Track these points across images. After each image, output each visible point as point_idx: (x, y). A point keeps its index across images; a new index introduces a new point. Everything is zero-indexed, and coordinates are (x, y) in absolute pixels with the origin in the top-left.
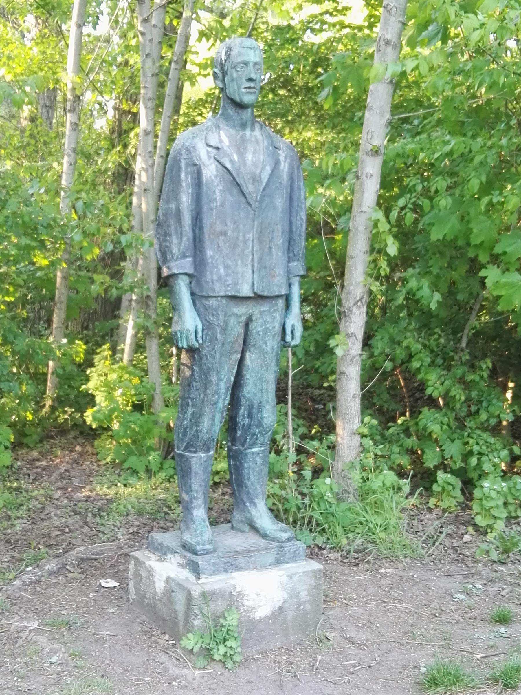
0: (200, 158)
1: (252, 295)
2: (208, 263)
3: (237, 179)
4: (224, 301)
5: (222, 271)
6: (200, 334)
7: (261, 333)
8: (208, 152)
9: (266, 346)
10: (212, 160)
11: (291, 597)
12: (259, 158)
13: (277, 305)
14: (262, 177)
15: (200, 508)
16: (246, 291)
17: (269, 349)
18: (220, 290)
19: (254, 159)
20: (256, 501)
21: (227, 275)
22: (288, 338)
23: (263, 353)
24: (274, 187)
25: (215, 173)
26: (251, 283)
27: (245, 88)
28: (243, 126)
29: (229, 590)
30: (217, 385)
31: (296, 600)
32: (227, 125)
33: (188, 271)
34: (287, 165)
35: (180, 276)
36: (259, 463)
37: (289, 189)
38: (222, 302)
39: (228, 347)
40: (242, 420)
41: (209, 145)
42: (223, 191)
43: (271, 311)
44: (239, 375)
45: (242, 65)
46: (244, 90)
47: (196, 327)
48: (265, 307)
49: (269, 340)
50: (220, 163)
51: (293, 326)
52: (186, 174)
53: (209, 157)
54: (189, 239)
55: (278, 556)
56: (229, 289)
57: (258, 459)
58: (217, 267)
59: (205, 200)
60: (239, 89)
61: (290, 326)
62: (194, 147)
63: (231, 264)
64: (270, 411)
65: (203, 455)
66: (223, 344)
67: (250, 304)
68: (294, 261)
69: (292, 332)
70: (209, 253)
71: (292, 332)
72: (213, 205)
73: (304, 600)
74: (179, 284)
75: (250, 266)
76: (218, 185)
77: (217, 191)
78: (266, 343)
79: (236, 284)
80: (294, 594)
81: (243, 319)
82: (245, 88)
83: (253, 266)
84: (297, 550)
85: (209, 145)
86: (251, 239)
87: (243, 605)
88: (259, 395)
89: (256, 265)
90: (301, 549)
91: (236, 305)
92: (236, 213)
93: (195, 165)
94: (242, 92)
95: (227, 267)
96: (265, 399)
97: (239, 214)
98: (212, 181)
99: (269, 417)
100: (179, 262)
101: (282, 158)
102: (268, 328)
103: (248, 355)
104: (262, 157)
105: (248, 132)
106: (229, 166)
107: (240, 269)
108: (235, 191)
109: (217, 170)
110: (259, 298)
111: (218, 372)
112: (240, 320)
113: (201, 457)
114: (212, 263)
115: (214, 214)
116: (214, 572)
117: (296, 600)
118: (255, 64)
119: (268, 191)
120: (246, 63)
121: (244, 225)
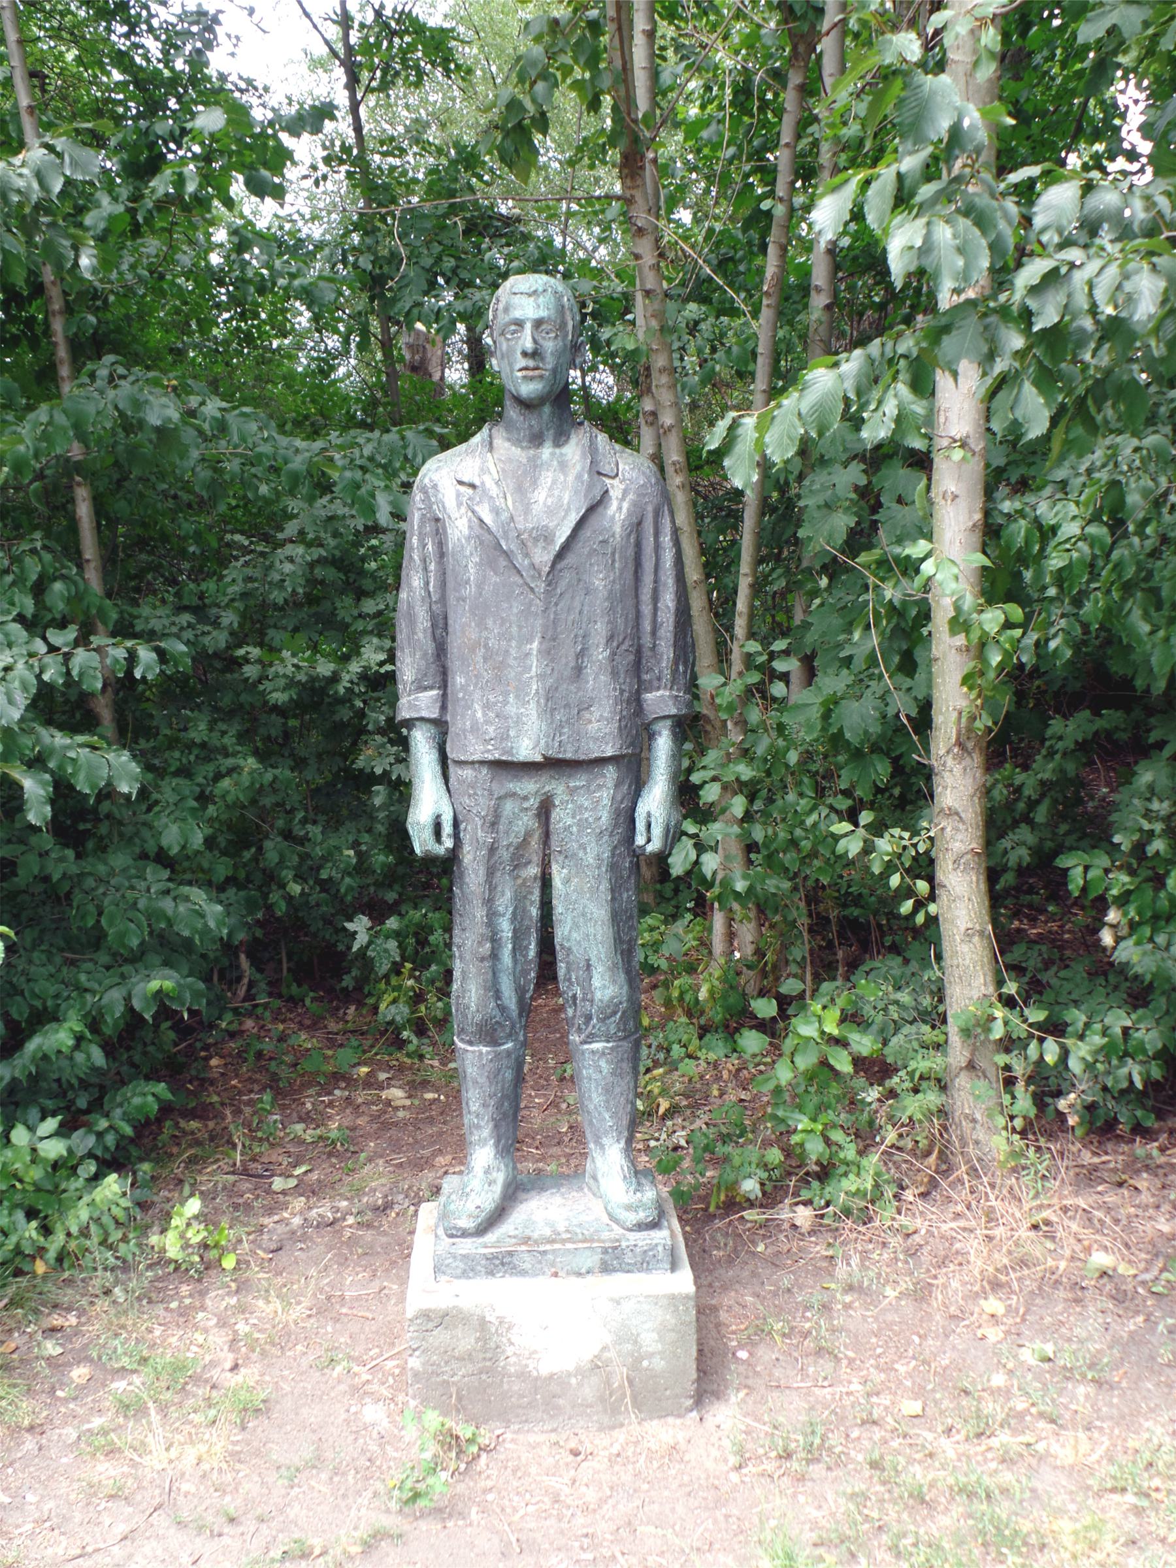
1: (539, 758)
2: (458, 700)
4: (484, 771)
5: (479, 714)
6: (447, 829)
7: (575, 829)
8: (458, 495)
10: (463, 509)
11: (620, 1340)
12: (560, 498)
15: (485, 1145)
16: (526, 749)
18: (476, 750)
22: (640, 840)
24: (586, 551)
25: (466, 532)
28: (536, 440)
29: (478, 1312)
31: (630, 1347)
32: (509, 440)
33: (425, 714)
34: (625, 505)
37: (630, 552)
41: (460, 483)
42: (479, 564)
44: (546, 906)
45: (513, 327)
46: (519, 374)
47: (438, 816)
48: (579, 781)
50: (473, 512)
51: (649, 815)
53: (459, 505)
54: (425, 654)
55: (607, 1257)
59: (450, 584)
60: (512, 371)
65: (484, 1049)
67: (545, 776)
73: (650, 1349)
77: (470, 565)
79: (504, 737)
80: (627, 1336)
81: (533, 802)
85: (460, 483)
87: (512, 1344)
90: (660, 1248)
93: (437, 520)
95: (487, 706)
101: (615, 494)
103: (555, 868)
105: (547, 451)
106: (488, 519)
107: (512, 709)
110: (553, 765)
113: (481, 1053)
116: (464, 1271)
117: (630, 1347)
119: (570, 559)
120: (520, 324)
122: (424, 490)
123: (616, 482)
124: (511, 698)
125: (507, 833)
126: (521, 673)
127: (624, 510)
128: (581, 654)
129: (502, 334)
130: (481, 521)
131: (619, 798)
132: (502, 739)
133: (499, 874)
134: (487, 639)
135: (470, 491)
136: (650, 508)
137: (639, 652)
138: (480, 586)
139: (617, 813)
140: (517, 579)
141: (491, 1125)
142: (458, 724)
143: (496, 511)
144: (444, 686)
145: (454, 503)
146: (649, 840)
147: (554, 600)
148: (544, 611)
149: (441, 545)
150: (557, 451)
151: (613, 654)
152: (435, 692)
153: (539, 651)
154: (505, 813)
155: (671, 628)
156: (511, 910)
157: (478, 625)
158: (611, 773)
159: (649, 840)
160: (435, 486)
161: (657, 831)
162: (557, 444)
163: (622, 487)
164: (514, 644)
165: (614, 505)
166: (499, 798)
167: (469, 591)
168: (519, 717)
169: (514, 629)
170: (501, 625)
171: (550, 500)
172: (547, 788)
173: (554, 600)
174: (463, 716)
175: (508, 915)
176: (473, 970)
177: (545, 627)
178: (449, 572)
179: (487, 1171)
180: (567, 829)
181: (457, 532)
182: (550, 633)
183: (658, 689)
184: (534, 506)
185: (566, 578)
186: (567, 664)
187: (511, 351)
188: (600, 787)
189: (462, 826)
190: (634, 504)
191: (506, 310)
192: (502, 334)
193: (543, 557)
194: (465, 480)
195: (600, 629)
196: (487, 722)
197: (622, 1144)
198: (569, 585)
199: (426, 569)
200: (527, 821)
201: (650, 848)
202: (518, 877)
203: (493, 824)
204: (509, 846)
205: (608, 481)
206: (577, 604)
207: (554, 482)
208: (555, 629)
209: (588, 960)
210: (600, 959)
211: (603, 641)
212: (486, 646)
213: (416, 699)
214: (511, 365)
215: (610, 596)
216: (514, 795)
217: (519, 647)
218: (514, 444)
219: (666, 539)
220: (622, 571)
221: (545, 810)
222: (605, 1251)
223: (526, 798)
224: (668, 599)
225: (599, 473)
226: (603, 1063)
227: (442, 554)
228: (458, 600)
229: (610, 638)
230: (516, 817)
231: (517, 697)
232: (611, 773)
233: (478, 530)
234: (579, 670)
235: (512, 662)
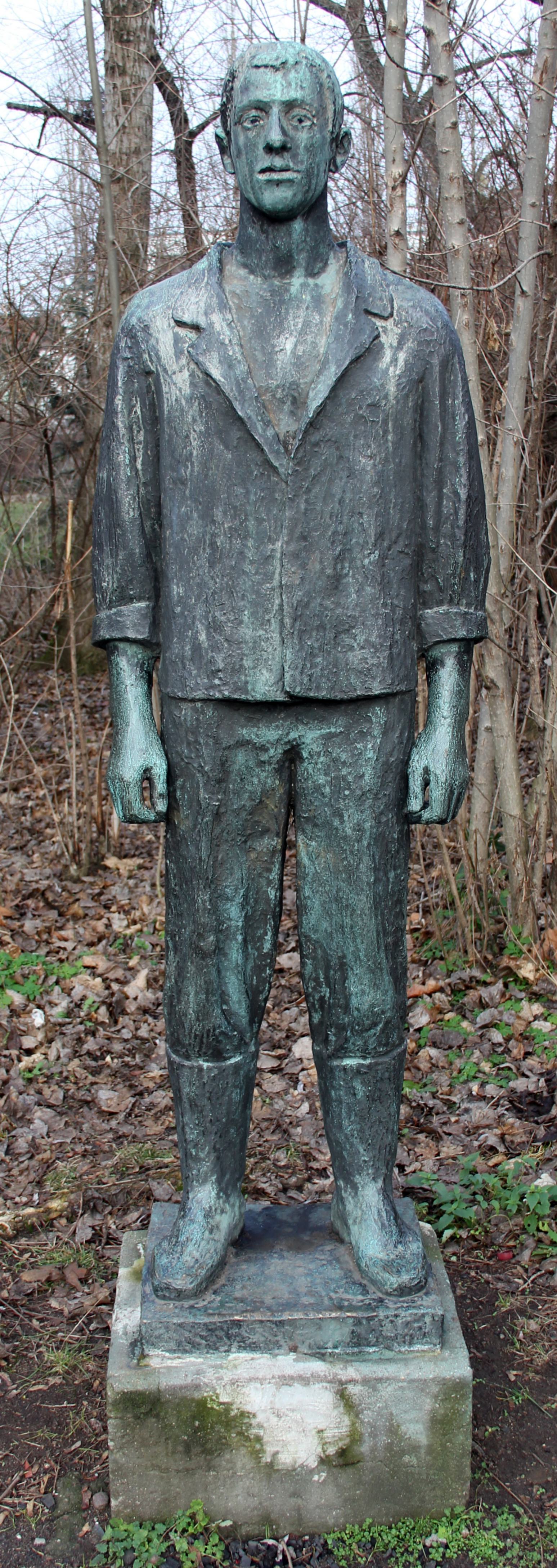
0: (159, 359)
1: (280, 697)
3: (237, 406)
4: (209, 712)
5: (203, 637)
6: (161, 786)
7: (327, 790)
8: (177, 340)
9: (342, 822)
12: (314, 345)
13: (369, 720)
14: (311, 394)
17: (349, 832)
19: (300, 349)
20: (358, 1179)
21: (215, 647)
23: (334, 838)
25: (187, 390)
26: (276, 668)
27: (263, 171)
30: (215, 910)
32: (245, 266)
33: (131, 634)
34: (402, 356)
35: (121, 645)
36: (360, 1094)
37: (408, 420)
38: (203, 712)
39: (232, 821)
40: (314, 988)
42: (205, 435)
45: (254, 113)
49: (347, 808)
51: (426, 771)
52: (129, 395)
53: (178, 353)
56: (217, 682)
57: (358, 1085)
58: (192, 626)
59: (166, 460)
60: (252, 172)
61: (421, 771)
62: (146, 328)
63: (223, 618)
64: (366, 981)
65: (206, 1065)
66: (217, 816)
68: (440, 603)
69: (426, 783)
70: (176, 590)
71: (426, 783)
72: (185, 472)
74: (117, 664)
75: (274, 625)
76: (194, 420)
77: (193, 435)
78: (341, 816)
79: (237, 669)
81: (275, 753)
82: (263, 171)
83: (282, 625)
85: (180, 323)
86: (278, 555)
88: (337, 937)
89: (287, 621)
91: (249, 719)
92: (240, 490)
93: (149, 373)
94: (258, 181)
95: (214, 627)
96: (352, 949)
97: (248, 492)
98: (182, 410)
99: (363, 992)
100: (114, 610)
101: (389, 340)
102: (344, 778)
104: (323, 343)
105: (297, 281)
106: (216, 373)
107: (247, 632)
108: (236, 434)
109: (193, 384)
111: (212, 883)
112: (264, 757)
113: (201, 1069)
114: (182, 613)
115: (187, 492)
118: (289, 106)
119: (330, 430)
120: (263, 107)
121: (259, 521)
123: (389, 324)
124: (246, 616)
125: (237, 793)
128: (339, 559)
129: (239, 122)
134: (214, 535)
135: (192, 335)
136: (436, 361)
138: (205, 465)
139: (386, 768)
140: (252, 455)
143: (228, 363)
145: (171, 351)
146: (426, 805)
150: (311, 281)
151: (383, 557)
152: (143, 604)
157: (202, 517)
162: (312, 273)
164: (250, 543)
165: (388, 354)
170: (234, 517)
172: (293, 735)
174: (182, 638)
175: (239, 899)
178: (164, 444)
181: (175, 392)
182: (299, 530)
184: (280, 356)
187: (251, 146)
188: (363, 735)
192: (239, 122)
194: (187, 318)
195: (369, 521)
196: (215, 647)
205: (379, 323)
207: (307, 324)
212: (213, 544)
215: (381, 479)
216: (243, 743)
218: (252, 272)
220: (397, 444)
225: (368, 312)
229: (380, 536)
231: (253, 614)
232: (378, 714)
233: (202, 390)
234: (336, 583)
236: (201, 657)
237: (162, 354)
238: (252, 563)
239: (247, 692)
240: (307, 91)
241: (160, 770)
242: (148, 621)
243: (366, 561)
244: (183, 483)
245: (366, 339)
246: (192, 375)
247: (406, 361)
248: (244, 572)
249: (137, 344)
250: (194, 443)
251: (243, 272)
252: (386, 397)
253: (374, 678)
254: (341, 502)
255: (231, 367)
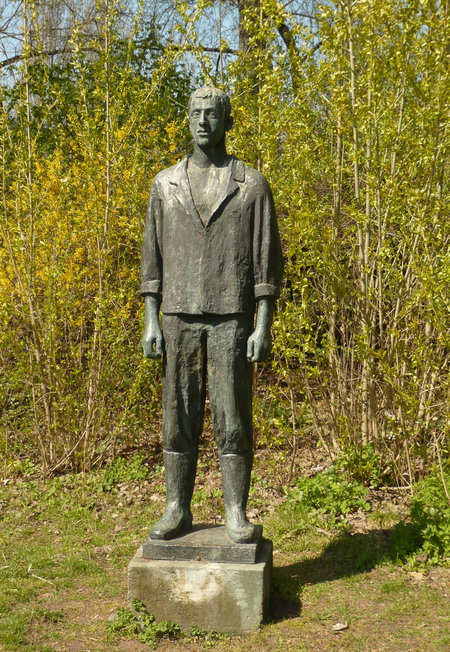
0: (163, 195)
5: (174, 291)
7: (218, 348)
8: (170, 189)
16: (194, 309)
20: (231, 502)
22: (249, 355)
25: (172, 206)
32: (195, 163)
33: (151, 290)
34: (246, 195)
41: (171, 183)
42: (177, 221)
43: (226, 328)
45: (196, 113)
53: (170, 193)
59: (164, 230)
65: (175, 453)
78: (222, 357)
84: (245, 552)
85: (171, 183)
90: (250, 551)
93: (160, 200)
95: (178, 288)
101: (242, 190)
103: (209, 366)
105: (213, 170)
106: (181, 201)
109: (174, 204)
113: (173, 455)
122: (155, 186)
123: (243, 184)
124: (189, 284)
125: (186, 348)
126: (194, 272)
127: (246, 197)
130: (179, 201)
131: (239, 333)
132: (184, 303)
133: (182, 368)
135: (175, 187)
136: (259, 196)
137: (251, 264)
141: (177, 491)
142: (166, 296)
144: (161, 277)
145: (168, 193)
146: (253, 355)
147: (210, 239)
148: (205, 244)
149: (162, 212)
151: (238, 265)
152: (156, 281)
153: (202, 262)
154: (185, 338)
155: (267, 254)
156: (187, 385)
157: (175, 250)
158: (234, 323)
159: (253, 355)
160: (160, 184)
161: (256, 350)
163: (246, 186)
164: (191, 259)
166: (183, 331)
167: (172, 234)
168: (192, 293)
169: (191, 252)
171: (211, 192)
172: (204, 328)
173: (210, 239)
174: (168, 292)
175: (186, 388)
176: (169, 413)
177: (205, 251)
178: (164, 225)
179: (174, 512)
180: (214, 347)
181: (168, 206)
182: (207, 254)
183: (261, 282)
185: (215, 227)
186: (215, 269)
188: (230, 328)
189: (166, 344)
190: (251, 195)
191: (194, 105)
193: (206, 218)
194: (173, 182)
195: (232, 253)
196: (178, 295)
197: (240, 505)
198: (217, 232)
199: (154, 223)
200: (196, 343)
201: (253, 358)
202: (191, 370)
203: (180, 344)
204: (187, 354)
205: (239, 184)
206: (221, 241)
207: (214, 184)
208: (210, 252)
209: (224, 412)
210: (228, 411)
211: (233, 259)
213: (148, 284)
214: (195, 129)
216: (188, 330)
217: (193, 260)
219: (267, 211)
220: (244, 226)
221: (204, 336)
222: (223, 550)
223: (195, 332)
224: (266, 240)
225: (235, 180)
226: (231, 464)
227: (162, 216)
228: (168, 237)
229: (236, 258)
230: (190, 340)
233: (177, 206)
234: (221, 272)
235: (189, 267)
236: (173, 298)
237: (165, 194)
238: (191, 266)
239: (188, 311)
240: (214, 105)
241: (159, 339)
242: (157, 287)
243: (231, 266)
244: (170, 238)
245: (233, 190)
246: (174, 201)
247: (248, 197)
248: (189, 269)
249: (156, 190)
250: (174, 224)
251: (194, 165)
252: (240, 208)
253: (233, 307)
254: (222, 245)
255: (186, 198)
